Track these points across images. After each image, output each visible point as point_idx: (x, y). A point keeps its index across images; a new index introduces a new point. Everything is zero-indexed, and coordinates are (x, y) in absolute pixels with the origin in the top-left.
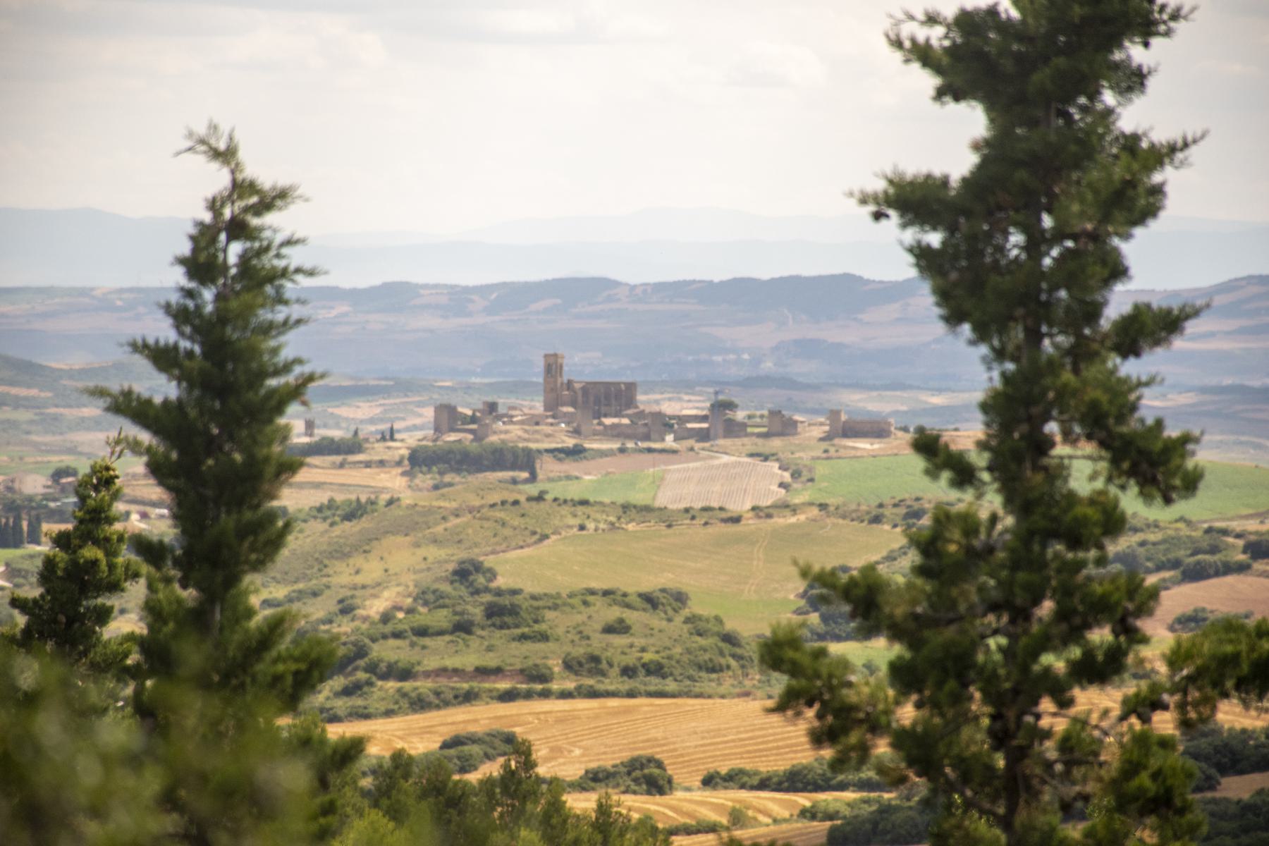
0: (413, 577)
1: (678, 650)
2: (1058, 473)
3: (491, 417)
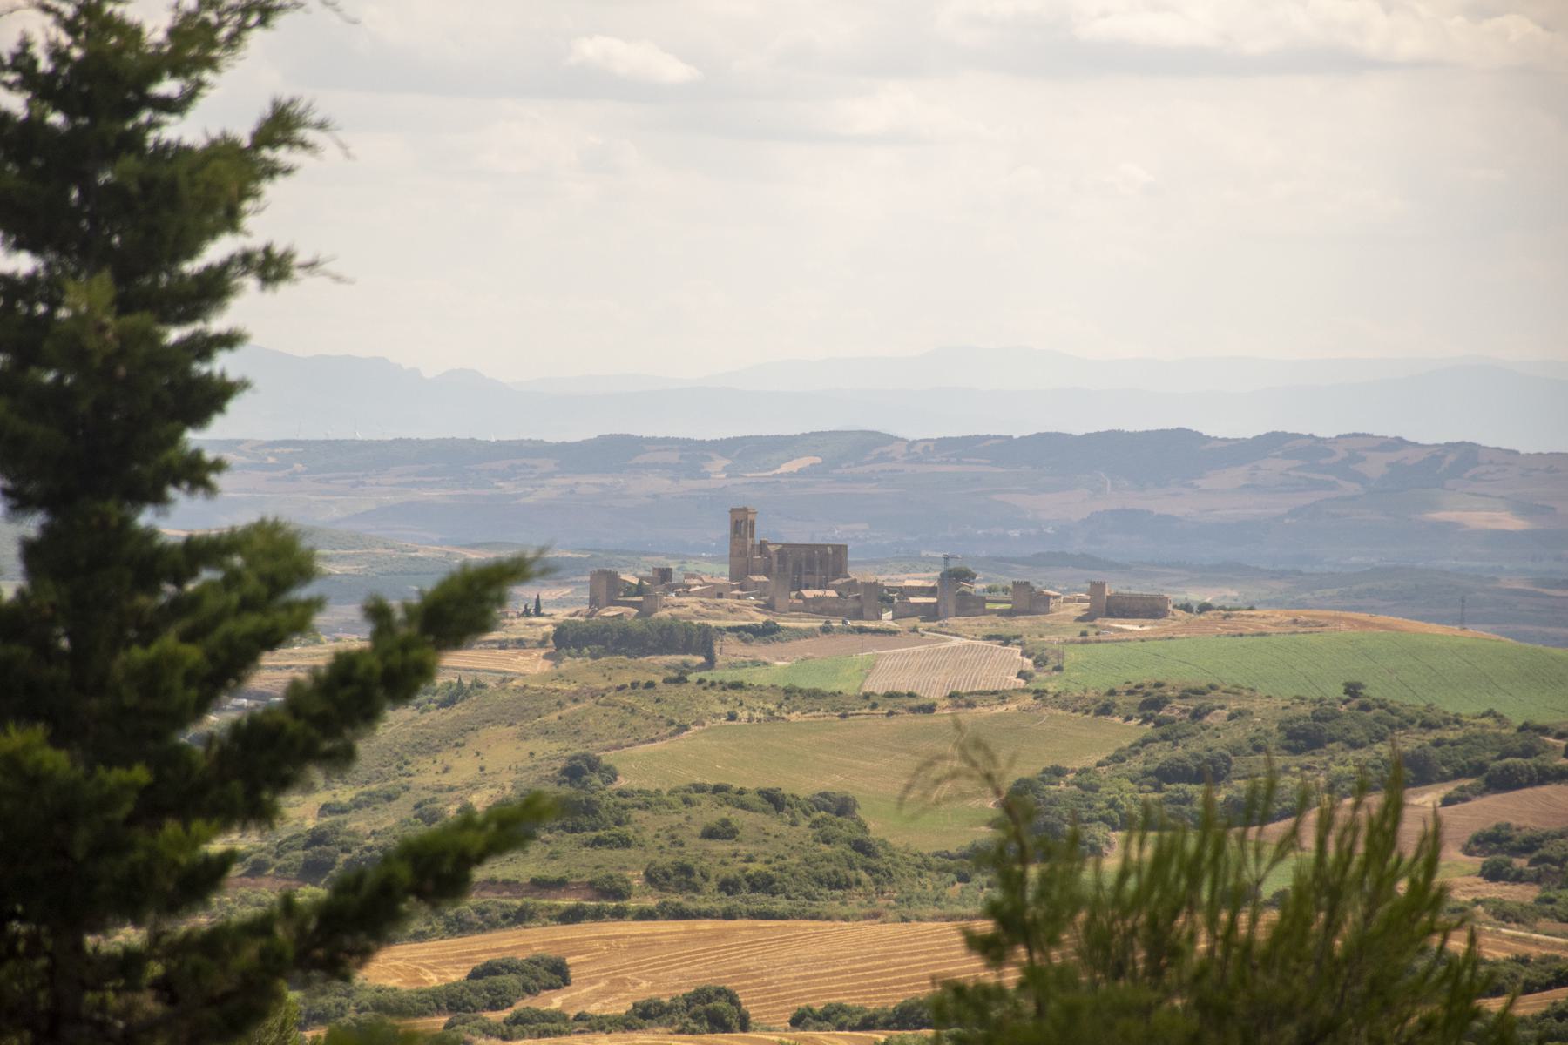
0: (513, 776)
3: (662, 587)
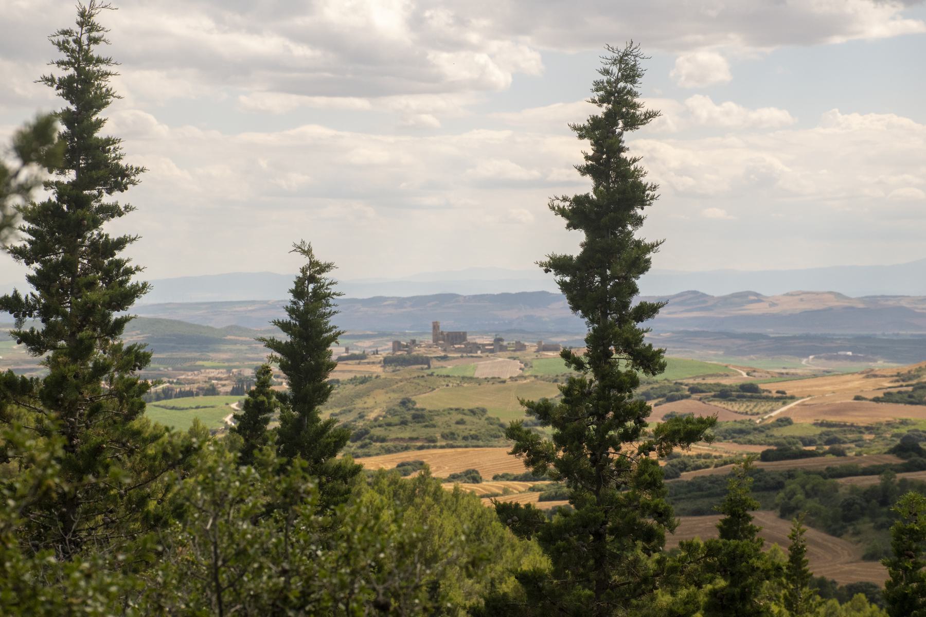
1: (483, 430)
2: (614, 365)
